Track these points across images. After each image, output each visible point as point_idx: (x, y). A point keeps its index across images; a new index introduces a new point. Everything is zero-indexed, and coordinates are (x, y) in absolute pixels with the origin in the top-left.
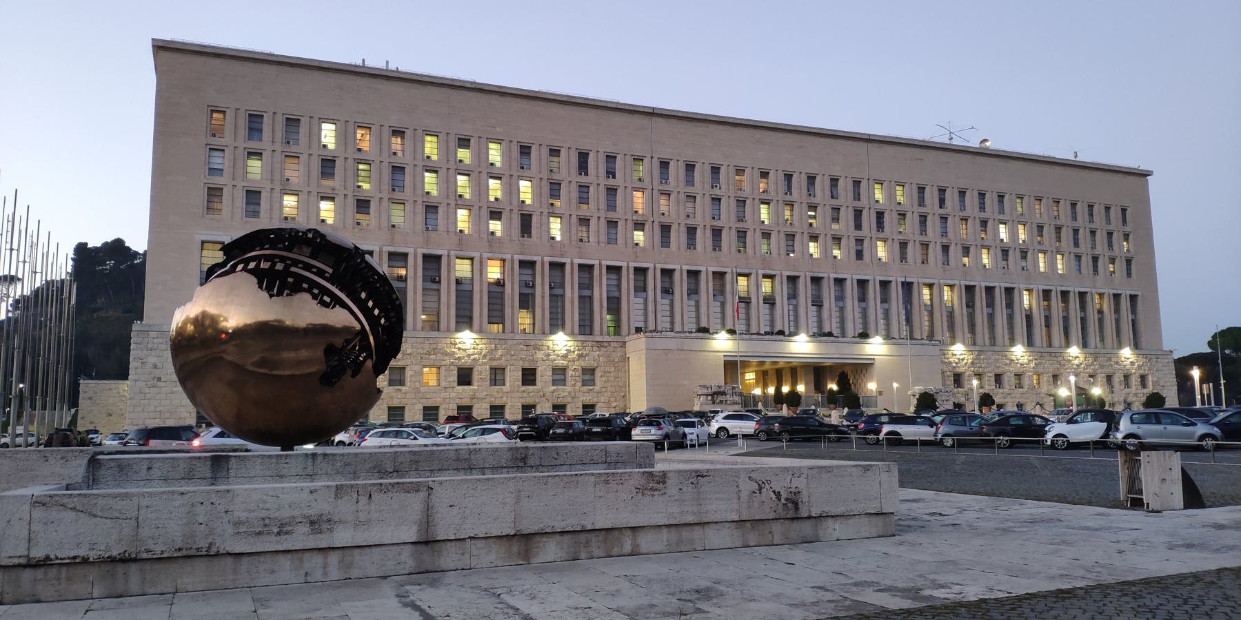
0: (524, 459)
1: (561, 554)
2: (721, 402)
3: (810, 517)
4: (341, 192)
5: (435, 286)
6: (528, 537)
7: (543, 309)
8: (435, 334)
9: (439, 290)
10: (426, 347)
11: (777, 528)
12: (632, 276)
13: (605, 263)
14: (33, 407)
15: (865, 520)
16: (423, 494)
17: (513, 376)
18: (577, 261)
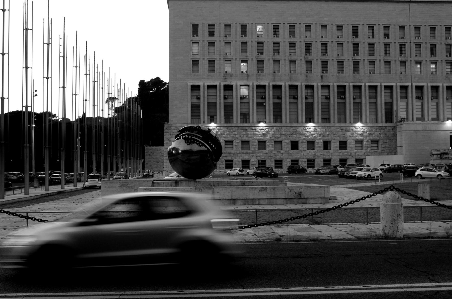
0: (244, 184)
1: (242, 203)
2: (446, 158)
3: (304, 198)
4: (250, 57)
5: (295, 101)
6: (234, 199)
7: (350, 110)
8: (295, 125)
9: (297, 103)
10: (291, 131)
11: (296, 201)
12: (399, 90)
13: (383, 84)
14: (126, 160)
15: (320, 199)
16: (212, 190)
17: (335, 145)
18: (368, 84)
